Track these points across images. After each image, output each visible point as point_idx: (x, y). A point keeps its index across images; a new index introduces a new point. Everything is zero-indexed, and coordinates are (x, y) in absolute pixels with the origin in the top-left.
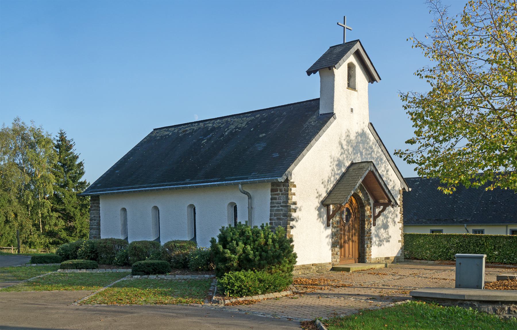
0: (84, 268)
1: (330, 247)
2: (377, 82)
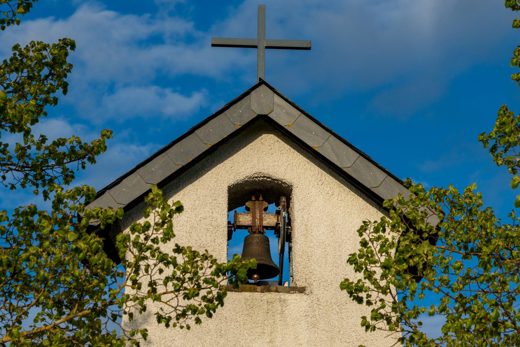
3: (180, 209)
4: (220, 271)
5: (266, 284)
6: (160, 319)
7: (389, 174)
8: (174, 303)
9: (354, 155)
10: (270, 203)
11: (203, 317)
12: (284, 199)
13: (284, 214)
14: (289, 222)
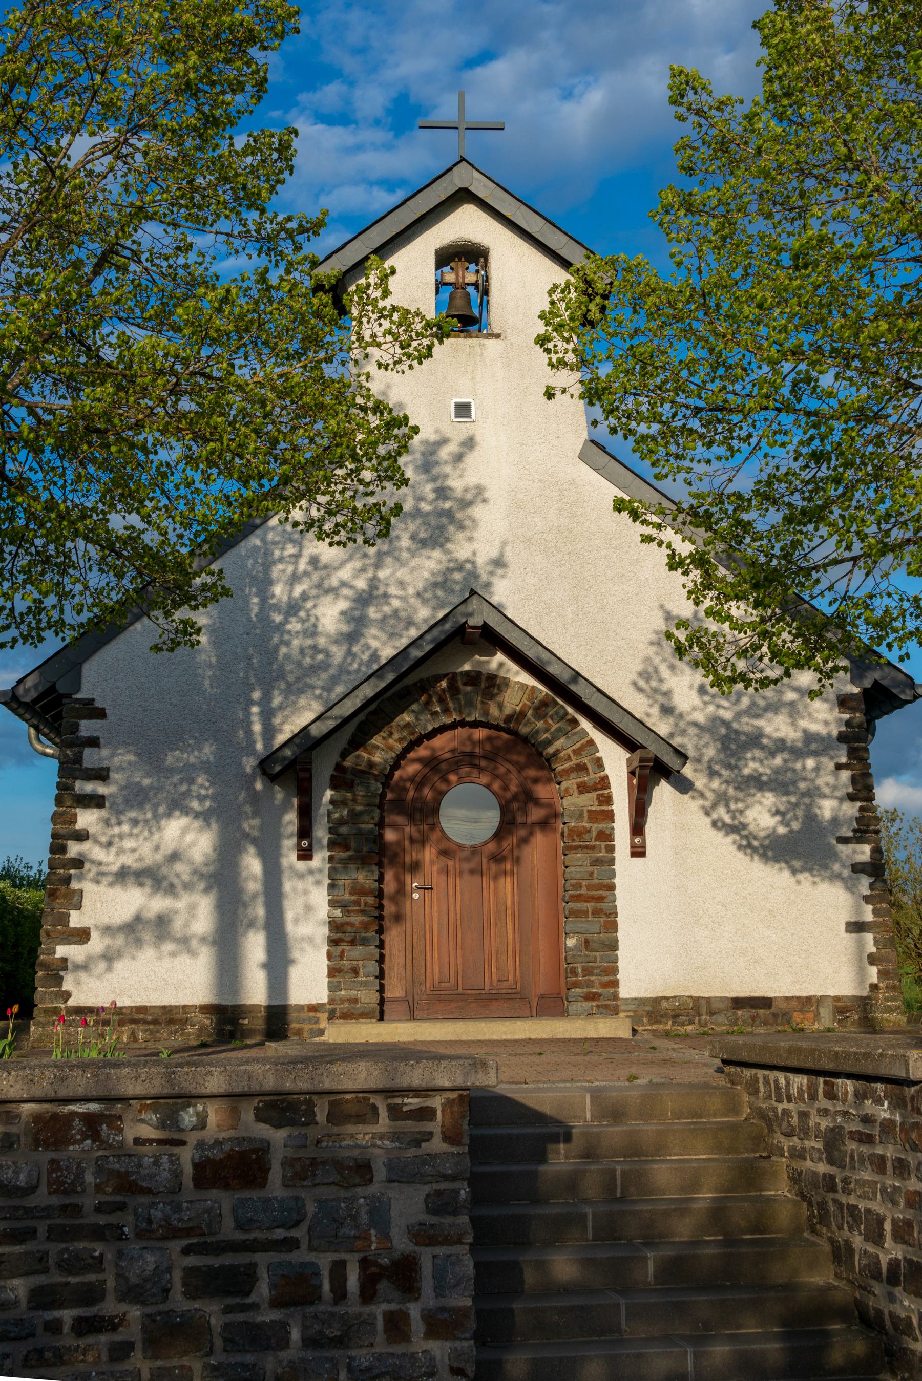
3: (393, 272)
4: (428, 325)
5: (467, 331)
6: (380, 365)
7: (498, 185)
8: (392, 351)
9: (565, 239)
10: (470, 263)
11: (415, 363)
12: (482, 260)
13: (483, 273)
14: (487, 279)
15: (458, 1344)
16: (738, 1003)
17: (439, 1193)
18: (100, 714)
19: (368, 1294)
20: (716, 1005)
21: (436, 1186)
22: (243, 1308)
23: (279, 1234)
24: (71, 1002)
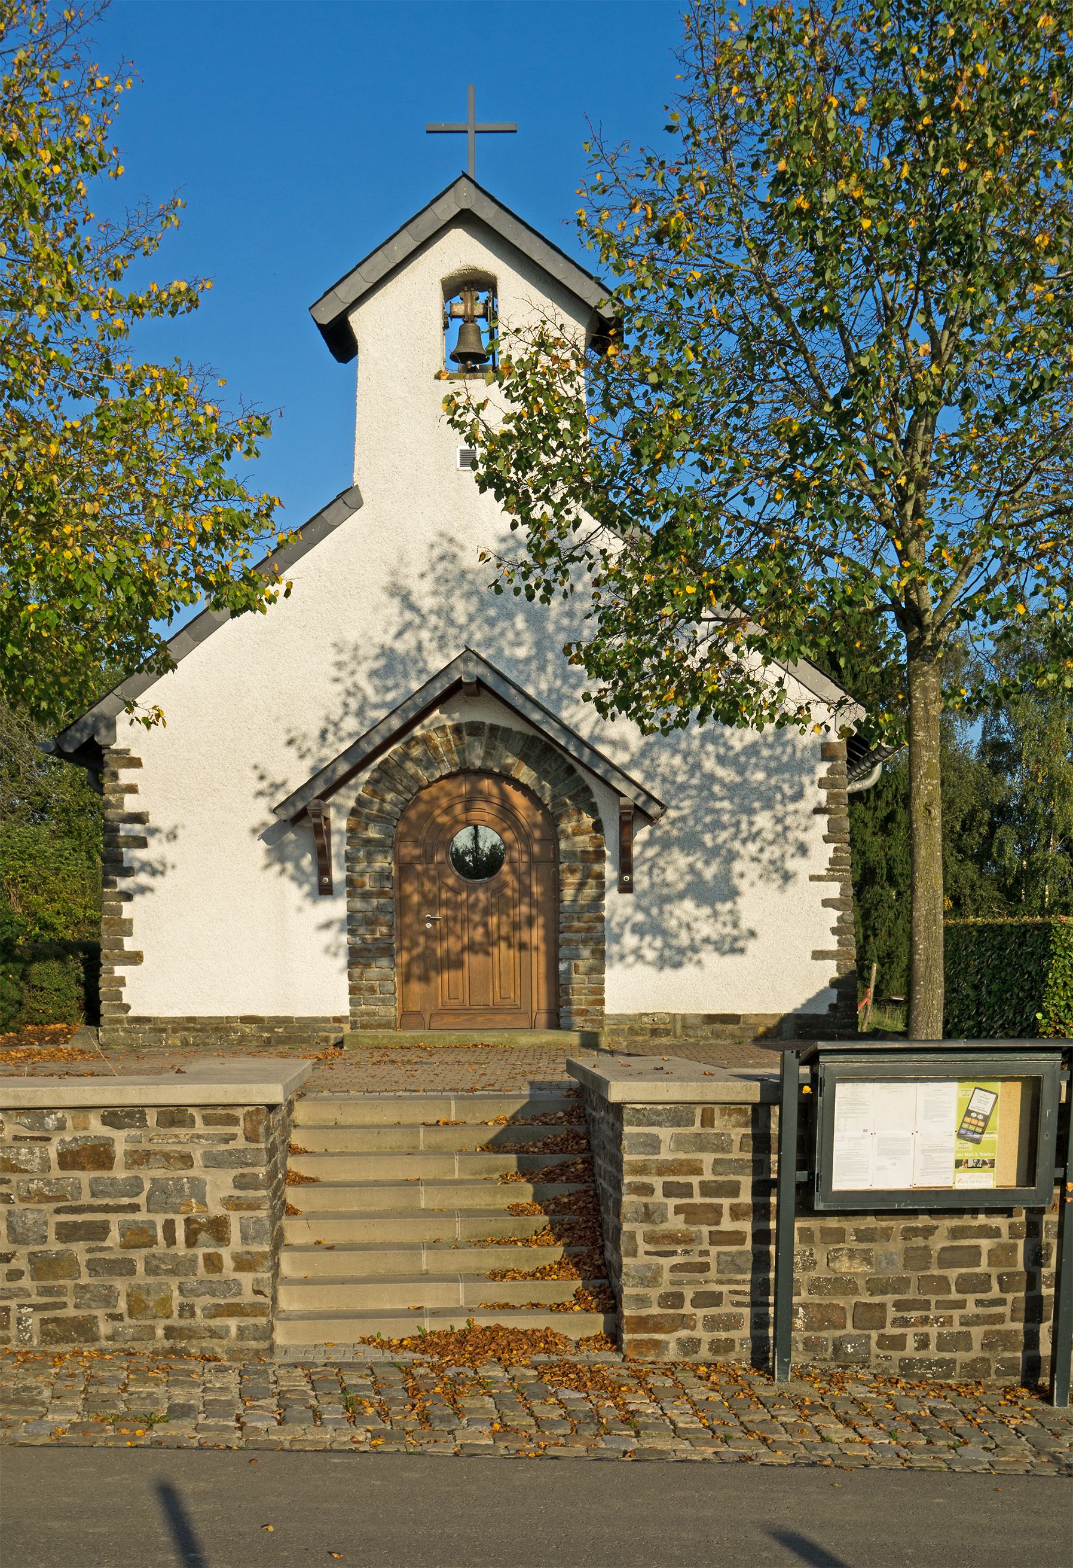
0: (849, 679)
1: (342, 961)
2: (812, 878)
15: (259, 1275)
16: (710, 1019)
17: (243, 1175)
18: (136, 763)
19: (191, 1241)
20: (690, 1021)
21: (241, 1171)
22: (102, 1249)
23: (125, 1201)
24: (131, 1013)
